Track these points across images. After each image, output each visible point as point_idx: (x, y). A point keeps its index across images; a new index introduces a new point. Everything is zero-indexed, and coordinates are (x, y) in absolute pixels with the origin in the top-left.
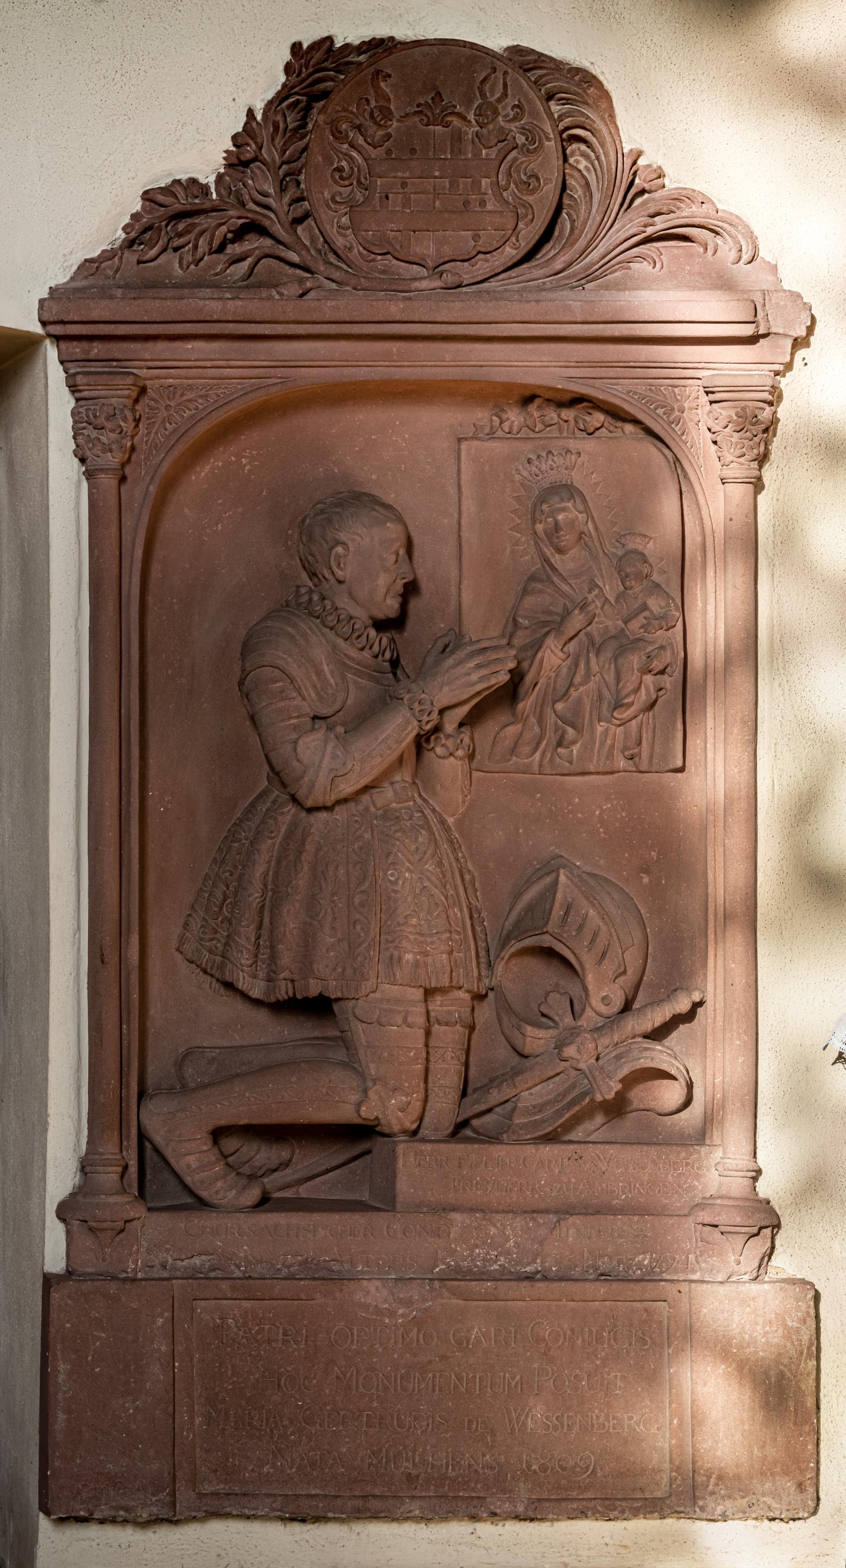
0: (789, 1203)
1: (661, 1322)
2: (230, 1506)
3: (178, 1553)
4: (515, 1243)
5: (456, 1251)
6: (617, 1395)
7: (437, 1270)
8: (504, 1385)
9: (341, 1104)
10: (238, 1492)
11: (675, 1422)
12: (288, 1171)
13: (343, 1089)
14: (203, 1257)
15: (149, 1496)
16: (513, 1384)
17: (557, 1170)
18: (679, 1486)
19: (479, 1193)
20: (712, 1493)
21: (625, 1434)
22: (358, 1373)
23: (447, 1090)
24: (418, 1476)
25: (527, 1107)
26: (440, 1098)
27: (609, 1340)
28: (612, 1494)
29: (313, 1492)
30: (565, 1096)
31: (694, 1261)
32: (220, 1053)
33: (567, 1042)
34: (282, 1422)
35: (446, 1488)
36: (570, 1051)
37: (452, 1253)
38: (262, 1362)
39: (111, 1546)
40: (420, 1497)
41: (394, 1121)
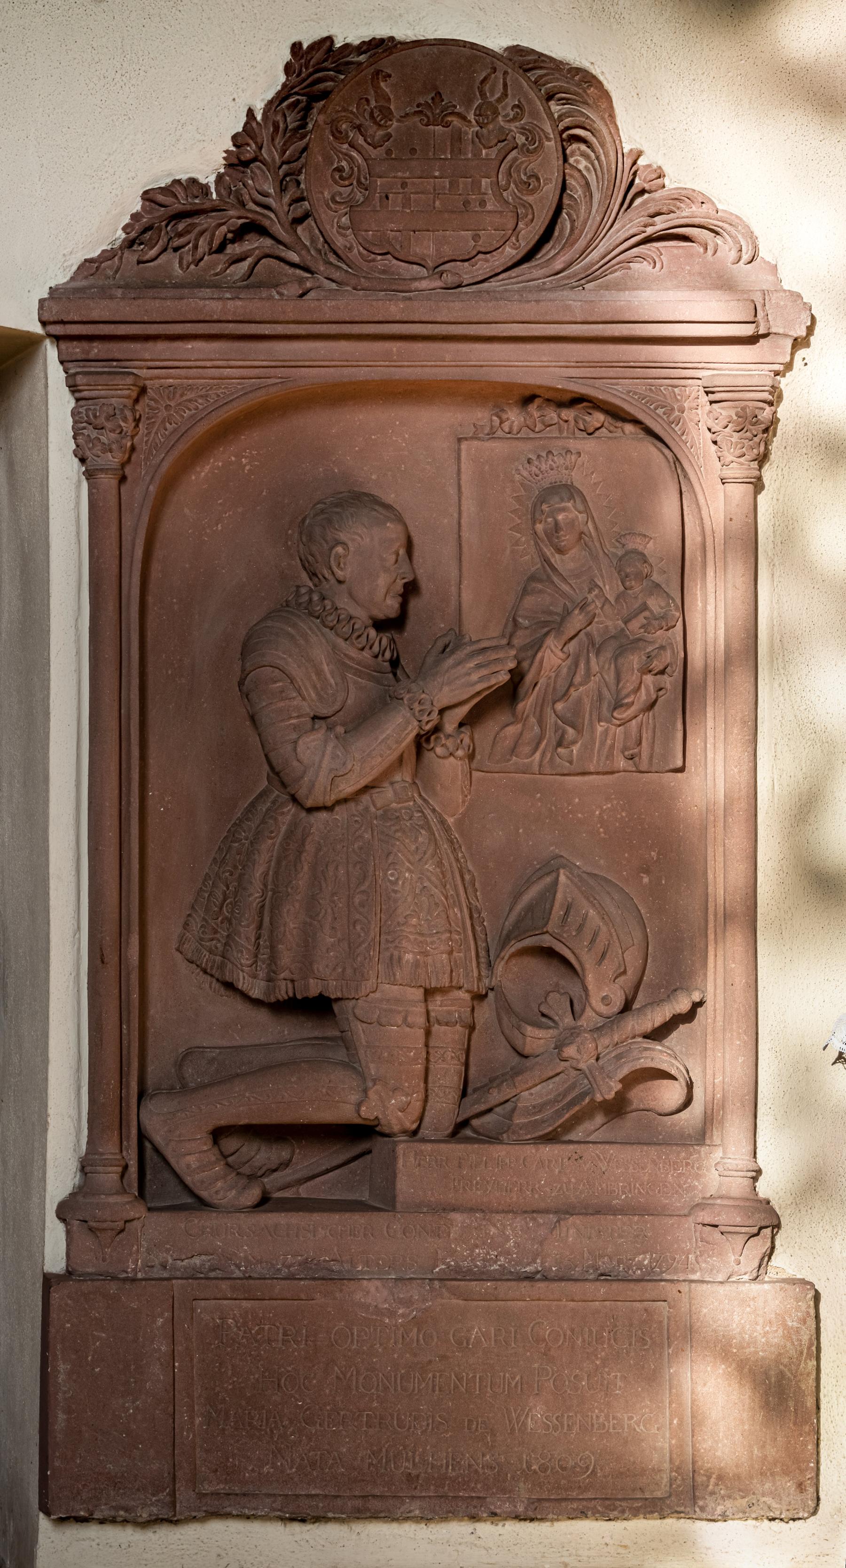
0: (789, 1203)
1: (661, 1322)
2: (230, 1506)
3: (178, 1553)
4: (515, 1243)
5: (456, 1251)
6: (617, 1395)
7: (437, 1270)
8: (504, 1385)
9: (341, 1104)
10: (238, 1492)
11: (675, 1422)
12: (288, 1171)
13: (343, 1089)
14: (203, 1257)
15: (149, 1496)
16: (513, 1384)
17: (557, 1170)
18: (679, 1486)
19: (479, 1193)
20: (712, 1493)
21: (625, 1434)
22: (358, 1373)
23: (447, 1090)
24: (418, 1476)
25: (527, 1107)
26: (440, 1098)
27: (609, 1340)
28: (612, 1494)
29: (313, 1492)
30: (565, 1096)
31: (694, 1261)
32: (220, 1053)
33: (567, 1042)
34: (282, 1422)
35: (446, 1488)
36: (570, 1051)
37: (452, 1253)
38: (262, 1362)
39: (111, 1546)
40: (420, 1497)
41: (394, 1121)
